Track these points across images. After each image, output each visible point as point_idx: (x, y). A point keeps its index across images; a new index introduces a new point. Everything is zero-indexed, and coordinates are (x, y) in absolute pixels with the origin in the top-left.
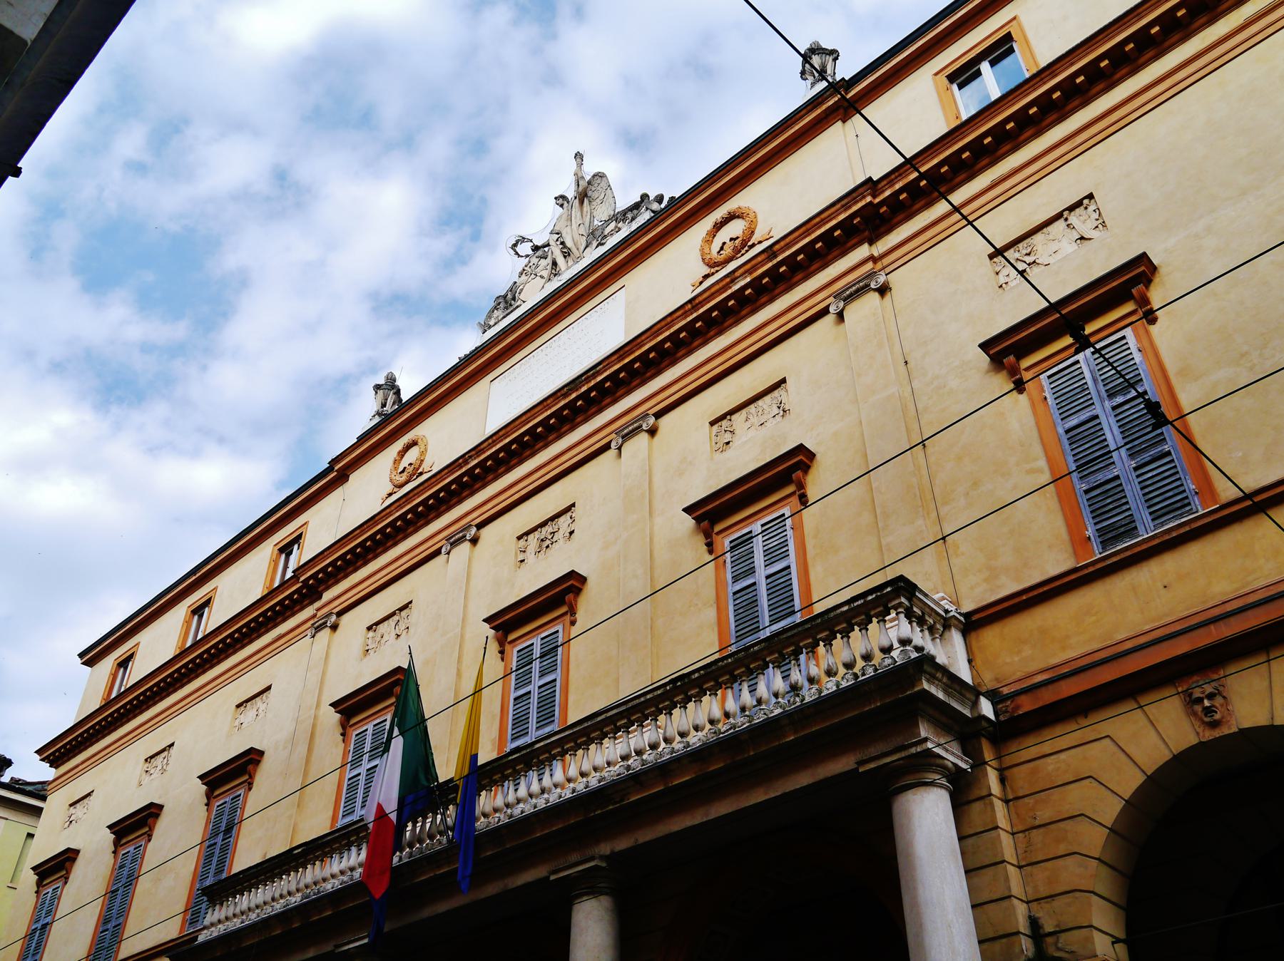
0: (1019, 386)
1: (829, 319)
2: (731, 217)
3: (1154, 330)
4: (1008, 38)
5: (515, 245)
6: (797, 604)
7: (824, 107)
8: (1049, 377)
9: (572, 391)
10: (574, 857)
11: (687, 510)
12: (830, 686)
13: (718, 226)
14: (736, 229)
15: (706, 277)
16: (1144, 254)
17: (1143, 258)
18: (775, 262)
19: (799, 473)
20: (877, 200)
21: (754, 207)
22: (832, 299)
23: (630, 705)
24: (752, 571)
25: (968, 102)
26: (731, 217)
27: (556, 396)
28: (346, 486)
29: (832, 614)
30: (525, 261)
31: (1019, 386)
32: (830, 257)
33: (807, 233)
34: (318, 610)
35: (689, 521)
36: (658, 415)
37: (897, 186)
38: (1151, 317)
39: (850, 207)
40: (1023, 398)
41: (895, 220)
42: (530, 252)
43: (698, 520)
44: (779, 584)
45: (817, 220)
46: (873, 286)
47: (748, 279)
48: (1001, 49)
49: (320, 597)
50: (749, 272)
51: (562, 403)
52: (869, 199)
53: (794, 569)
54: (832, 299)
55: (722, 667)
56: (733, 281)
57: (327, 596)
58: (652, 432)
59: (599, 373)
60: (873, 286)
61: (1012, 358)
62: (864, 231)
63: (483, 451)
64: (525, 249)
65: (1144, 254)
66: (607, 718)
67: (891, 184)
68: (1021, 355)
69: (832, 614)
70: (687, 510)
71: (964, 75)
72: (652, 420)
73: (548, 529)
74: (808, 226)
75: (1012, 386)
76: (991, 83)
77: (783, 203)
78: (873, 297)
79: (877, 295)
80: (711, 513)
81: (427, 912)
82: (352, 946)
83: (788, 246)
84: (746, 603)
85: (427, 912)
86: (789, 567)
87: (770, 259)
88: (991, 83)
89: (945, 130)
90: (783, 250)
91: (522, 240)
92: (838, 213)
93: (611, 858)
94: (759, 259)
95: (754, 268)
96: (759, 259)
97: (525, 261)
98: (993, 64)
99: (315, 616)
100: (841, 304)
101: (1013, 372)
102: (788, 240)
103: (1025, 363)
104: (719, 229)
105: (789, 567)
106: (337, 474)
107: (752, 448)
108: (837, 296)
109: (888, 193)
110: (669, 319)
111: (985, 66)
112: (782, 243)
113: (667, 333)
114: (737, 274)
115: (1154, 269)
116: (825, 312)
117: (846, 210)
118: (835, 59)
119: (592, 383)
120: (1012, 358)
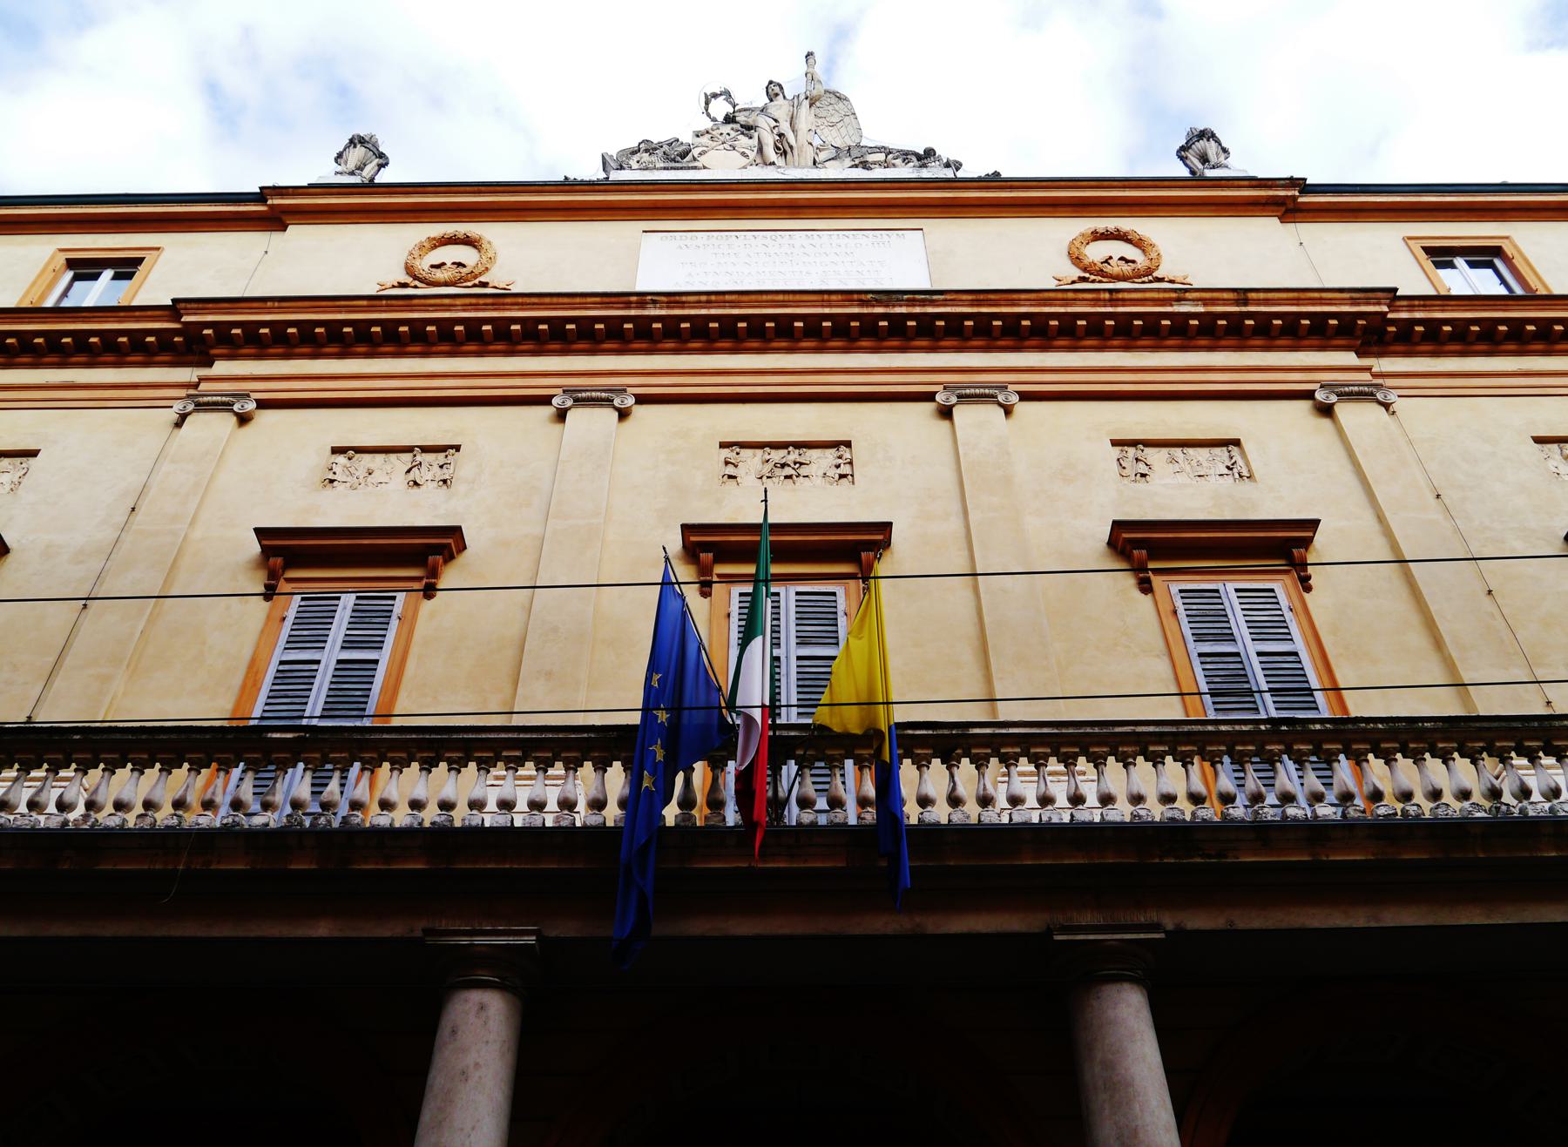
0: (269, 594)
1: (546, 412)
2: (468, 241)
3: (427, 606)
4: (138, 262)
5: (715, 96)
6: (371, 708)
7: (1271, 193)
8: (798, 593)
9: (879, 303)
10: (1087, 918)
11: (259, 532)
12: (1456, 808)
13: (1099, 236)
14: (1096, 252)
15: (404, 285)
16: (890, 524)
17: (455, 532)
18: (1244, 309)
19: (440, 559)
20: (1390, 316)
21: (495, 243)
22: (560, 391)
23: (1111, 730)
24: (319, 642)
25: (1413, 279)
26: (468, 241)
27: (848, 295)
28: (276, 238)
29: (1557, 724)
30: (709, 124)
31: (269, 594)
32: (1306, 342)
33: (1297, 302)
34: (201, 380)
35: (255, 548)
36: (263, 405)
37: (1418, 315)
38: (429, 591)
39: (1358, 304)
40: (260, 607)
41: (1392, 348)
42: (721, 118)
43: (267, 552)
44: (353, 674)
45: (1316, 295)
46: (236, 408)
47: (1201, 309)
48: (126, 268)
49: (210, 365)
50: (1205, 302)
51: (856, 310)
52: (1385, 309)
53: (381, 669)
54: (560, 391)
55: (1365, 730)
56: (1178, 300)
57: (221, 368)
58: (243, 419)
59: (933, 303)
60: (236, 408)
61: (279, 560)
62: (1357, 338)
63: (682, 305)
64: (720, 108)
65: (890, 524)
66: (1134, 733)
67: (1411, 308)
68: (720, 559)
69: (1557, 724)
70: (259, 532)
71: (1441, 256)
72: (251, 406)
73: (794, 455)
74: (1302, 295)
75: (261, 589)
76: (99, 292)
77: (529, 260)
78: (230, 420)
79: (234, 419)
80: (288, 553)
81: (698, 927)
82: (480, 940)
83: (1267, 302)
84: (294, 678)
85: (698, 927)
86: (376, 662)
87: (1237, 302)
88: (99, 292)
89: (13, 305)
90: (1258, 302)
91: (727, 94)
92: (1342, 302)
93: (1180, 933)
94: (1225, 295)
95: (1213, 302)
96: (1225, 295)
97: (709, 124)
98: (116, 277)
99: (196, 386)
100: (569, 403)
101: (273, 576)
102: (1270, 295)
103: (721, 569)
104: (435, 247)
105: (376, 662)
106: (269, 211)
107: (385, 501)
108: (567, 391)
109: (1404, 315)
110: (704, 298)
111: (108, 274)
112: (1262, 295)
113: (1062, 310)
114: (1188, 295)
115: (462, 547)
116: (545, 401)
117: (972, 306)
118: (381, 166)
119: (918, 310)
120: (711, 555)
